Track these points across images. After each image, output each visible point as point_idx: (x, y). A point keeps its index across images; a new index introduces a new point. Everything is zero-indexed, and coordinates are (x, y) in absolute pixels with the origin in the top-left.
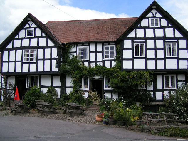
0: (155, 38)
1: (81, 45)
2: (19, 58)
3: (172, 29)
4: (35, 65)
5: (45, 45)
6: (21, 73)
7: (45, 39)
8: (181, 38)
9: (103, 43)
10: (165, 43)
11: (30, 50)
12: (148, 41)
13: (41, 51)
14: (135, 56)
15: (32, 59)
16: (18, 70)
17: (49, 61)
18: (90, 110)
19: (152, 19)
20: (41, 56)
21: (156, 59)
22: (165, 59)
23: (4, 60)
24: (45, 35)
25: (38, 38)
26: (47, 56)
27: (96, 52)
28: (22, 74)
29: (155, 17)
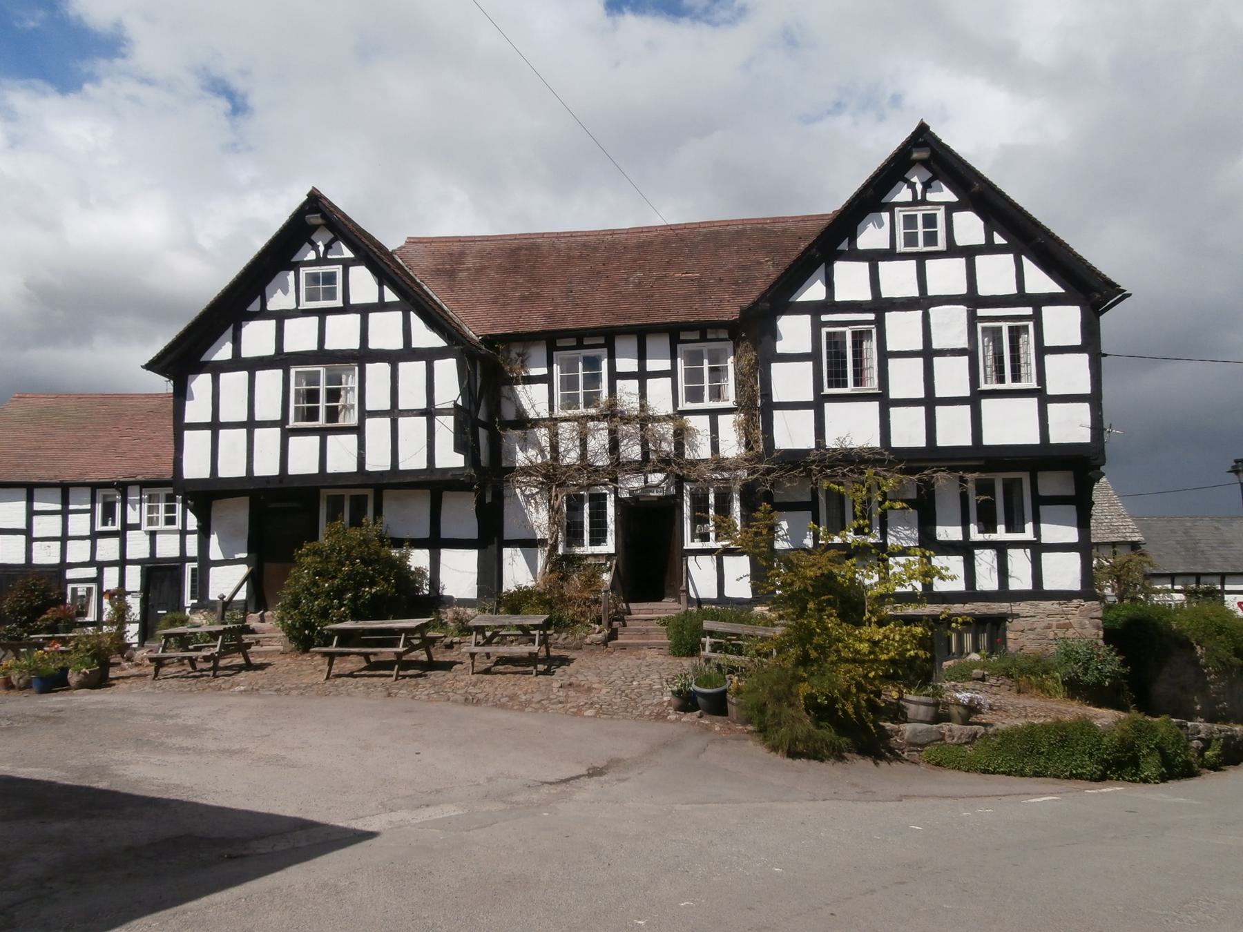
0: (923, 302)
1: (572, 342)
2: (268, 408)
3: (1010, 258)
4: (353, 438)
5: (397, 344)
6: (281, 481)
7: (398, 316)
8: (1052, 299)
9: (675, 334)
10: (973, 320)
11: (322, 370)
12: (891, 318)
13: (378, 373)
14: (827, 391)
15: (333, 414)
16: (267, 466)
17: (207, 434)
18: (624, 647)
19: (910, 212)
20: (378, 398)
21: (930, 402)
22: (975, 399)
23: (189, 418)
24: (397, 299)
25: (364, 310)
26: (413, 396)
27: (642, 376)
28: (284, 485)
29: (924, 202)
